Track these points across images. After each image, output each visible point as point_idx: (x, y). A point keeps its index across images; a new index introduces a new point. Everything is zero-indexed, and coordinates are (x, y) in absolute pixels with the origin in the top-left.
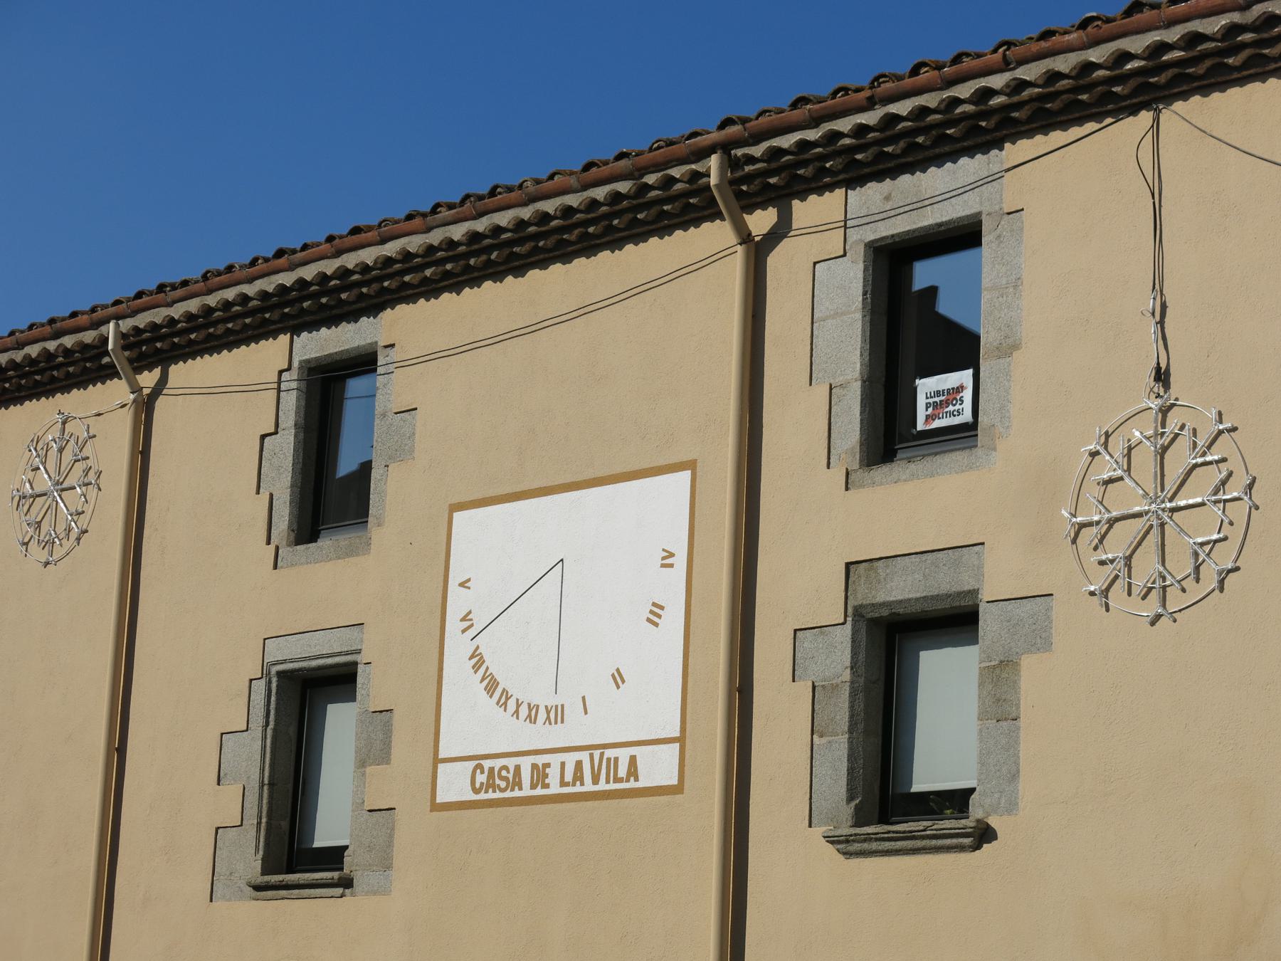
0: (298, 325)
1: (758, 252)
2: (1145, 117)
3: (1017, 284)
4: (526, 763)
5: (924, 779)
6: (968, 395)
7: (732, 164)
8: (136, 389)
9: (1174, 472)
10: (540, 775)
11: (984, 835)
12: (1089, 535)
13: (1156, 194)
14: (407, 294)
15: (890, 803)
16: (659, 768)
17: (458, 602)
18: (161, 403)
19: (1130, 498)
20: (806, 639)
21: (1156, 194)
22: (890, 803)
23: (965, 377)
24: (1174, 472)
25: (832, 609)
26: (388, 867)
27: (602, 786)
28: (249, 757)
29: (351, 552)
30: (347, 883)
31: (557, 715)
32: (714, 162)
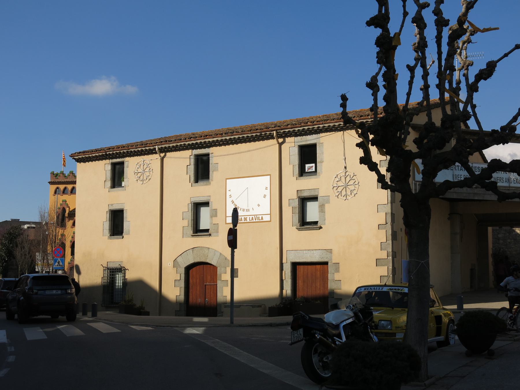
0: (193, 149)
1: (280, 145)
2: (342, 132)
3: (323, 153)
4: (260, 216)
5: (201, 228)
6: (314, 167)
7: (277, 133)
8: (160, 156)
9: (347, 180)
10: (245, 219)
11: (321, 228)
12: (335, 188)
13: (344, 143)
14: (216, 146)
15: (304, 223)
16: (267, 218)
17: (228, 193)
18: (165, 159)
19: (340, 184)
20: (291, 201)
21: (344, 143)
22: (304, 223)
23: (314, 165)
24: (347, 180)
25: (295, 196)
26: (218, 232)
27: (257, 221)
28: (189, 216)
29: (206, 185)
30: (210, 235)
31: (248, 210)
32: (275, 132)
